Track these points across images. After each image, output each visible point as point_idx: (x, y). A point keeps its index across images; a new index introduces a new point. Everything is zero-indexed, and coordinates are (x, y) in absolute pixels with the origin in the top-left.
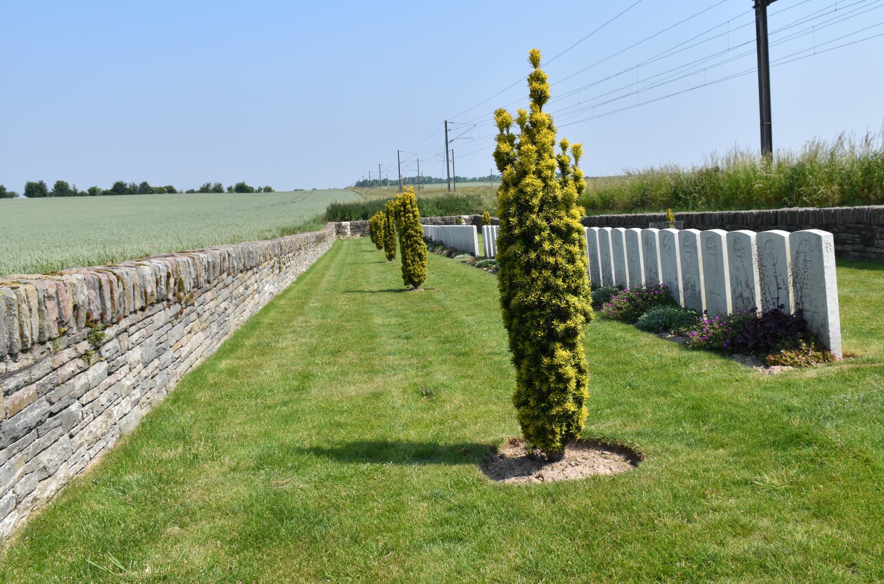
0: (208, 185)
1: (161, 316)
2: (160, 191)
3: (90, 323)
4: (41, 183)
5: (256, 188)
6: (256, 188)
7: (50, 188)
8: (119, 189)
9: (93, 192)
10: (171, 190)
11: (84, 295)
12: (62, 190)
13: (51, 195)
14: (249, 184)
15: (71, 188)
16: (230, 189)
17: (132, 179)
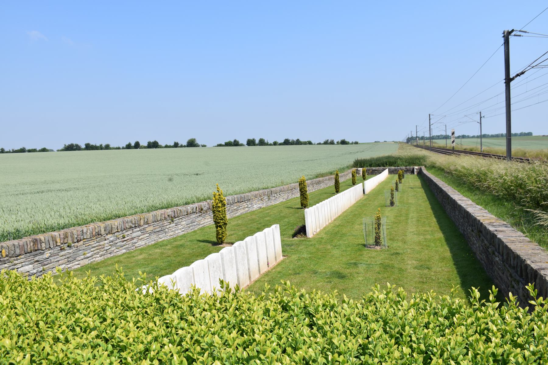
0: (328, 141)
1: (193, 216)
2: (305, 143)
3: (172, 217)
4: (254, 139)
5: (351, 142)
6: (351, 142)
7: (257, 142)
8: (287, 142)
9: (275, 144)
10: (310, 143)
11: (170, 213)
12: (262, 143)
13: (257, 145)
14: (347, 140)
15: (266, 142)
16: (338, 142)
17: (293, 138)
